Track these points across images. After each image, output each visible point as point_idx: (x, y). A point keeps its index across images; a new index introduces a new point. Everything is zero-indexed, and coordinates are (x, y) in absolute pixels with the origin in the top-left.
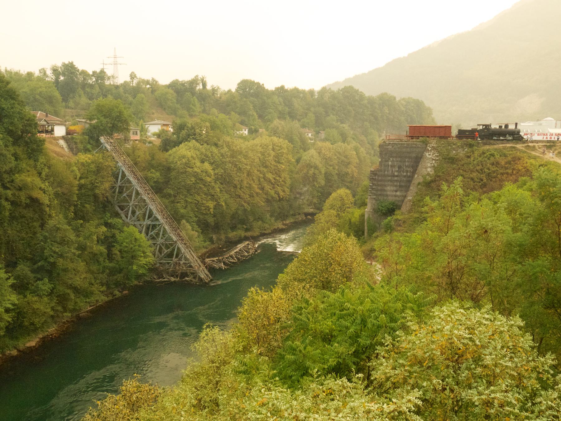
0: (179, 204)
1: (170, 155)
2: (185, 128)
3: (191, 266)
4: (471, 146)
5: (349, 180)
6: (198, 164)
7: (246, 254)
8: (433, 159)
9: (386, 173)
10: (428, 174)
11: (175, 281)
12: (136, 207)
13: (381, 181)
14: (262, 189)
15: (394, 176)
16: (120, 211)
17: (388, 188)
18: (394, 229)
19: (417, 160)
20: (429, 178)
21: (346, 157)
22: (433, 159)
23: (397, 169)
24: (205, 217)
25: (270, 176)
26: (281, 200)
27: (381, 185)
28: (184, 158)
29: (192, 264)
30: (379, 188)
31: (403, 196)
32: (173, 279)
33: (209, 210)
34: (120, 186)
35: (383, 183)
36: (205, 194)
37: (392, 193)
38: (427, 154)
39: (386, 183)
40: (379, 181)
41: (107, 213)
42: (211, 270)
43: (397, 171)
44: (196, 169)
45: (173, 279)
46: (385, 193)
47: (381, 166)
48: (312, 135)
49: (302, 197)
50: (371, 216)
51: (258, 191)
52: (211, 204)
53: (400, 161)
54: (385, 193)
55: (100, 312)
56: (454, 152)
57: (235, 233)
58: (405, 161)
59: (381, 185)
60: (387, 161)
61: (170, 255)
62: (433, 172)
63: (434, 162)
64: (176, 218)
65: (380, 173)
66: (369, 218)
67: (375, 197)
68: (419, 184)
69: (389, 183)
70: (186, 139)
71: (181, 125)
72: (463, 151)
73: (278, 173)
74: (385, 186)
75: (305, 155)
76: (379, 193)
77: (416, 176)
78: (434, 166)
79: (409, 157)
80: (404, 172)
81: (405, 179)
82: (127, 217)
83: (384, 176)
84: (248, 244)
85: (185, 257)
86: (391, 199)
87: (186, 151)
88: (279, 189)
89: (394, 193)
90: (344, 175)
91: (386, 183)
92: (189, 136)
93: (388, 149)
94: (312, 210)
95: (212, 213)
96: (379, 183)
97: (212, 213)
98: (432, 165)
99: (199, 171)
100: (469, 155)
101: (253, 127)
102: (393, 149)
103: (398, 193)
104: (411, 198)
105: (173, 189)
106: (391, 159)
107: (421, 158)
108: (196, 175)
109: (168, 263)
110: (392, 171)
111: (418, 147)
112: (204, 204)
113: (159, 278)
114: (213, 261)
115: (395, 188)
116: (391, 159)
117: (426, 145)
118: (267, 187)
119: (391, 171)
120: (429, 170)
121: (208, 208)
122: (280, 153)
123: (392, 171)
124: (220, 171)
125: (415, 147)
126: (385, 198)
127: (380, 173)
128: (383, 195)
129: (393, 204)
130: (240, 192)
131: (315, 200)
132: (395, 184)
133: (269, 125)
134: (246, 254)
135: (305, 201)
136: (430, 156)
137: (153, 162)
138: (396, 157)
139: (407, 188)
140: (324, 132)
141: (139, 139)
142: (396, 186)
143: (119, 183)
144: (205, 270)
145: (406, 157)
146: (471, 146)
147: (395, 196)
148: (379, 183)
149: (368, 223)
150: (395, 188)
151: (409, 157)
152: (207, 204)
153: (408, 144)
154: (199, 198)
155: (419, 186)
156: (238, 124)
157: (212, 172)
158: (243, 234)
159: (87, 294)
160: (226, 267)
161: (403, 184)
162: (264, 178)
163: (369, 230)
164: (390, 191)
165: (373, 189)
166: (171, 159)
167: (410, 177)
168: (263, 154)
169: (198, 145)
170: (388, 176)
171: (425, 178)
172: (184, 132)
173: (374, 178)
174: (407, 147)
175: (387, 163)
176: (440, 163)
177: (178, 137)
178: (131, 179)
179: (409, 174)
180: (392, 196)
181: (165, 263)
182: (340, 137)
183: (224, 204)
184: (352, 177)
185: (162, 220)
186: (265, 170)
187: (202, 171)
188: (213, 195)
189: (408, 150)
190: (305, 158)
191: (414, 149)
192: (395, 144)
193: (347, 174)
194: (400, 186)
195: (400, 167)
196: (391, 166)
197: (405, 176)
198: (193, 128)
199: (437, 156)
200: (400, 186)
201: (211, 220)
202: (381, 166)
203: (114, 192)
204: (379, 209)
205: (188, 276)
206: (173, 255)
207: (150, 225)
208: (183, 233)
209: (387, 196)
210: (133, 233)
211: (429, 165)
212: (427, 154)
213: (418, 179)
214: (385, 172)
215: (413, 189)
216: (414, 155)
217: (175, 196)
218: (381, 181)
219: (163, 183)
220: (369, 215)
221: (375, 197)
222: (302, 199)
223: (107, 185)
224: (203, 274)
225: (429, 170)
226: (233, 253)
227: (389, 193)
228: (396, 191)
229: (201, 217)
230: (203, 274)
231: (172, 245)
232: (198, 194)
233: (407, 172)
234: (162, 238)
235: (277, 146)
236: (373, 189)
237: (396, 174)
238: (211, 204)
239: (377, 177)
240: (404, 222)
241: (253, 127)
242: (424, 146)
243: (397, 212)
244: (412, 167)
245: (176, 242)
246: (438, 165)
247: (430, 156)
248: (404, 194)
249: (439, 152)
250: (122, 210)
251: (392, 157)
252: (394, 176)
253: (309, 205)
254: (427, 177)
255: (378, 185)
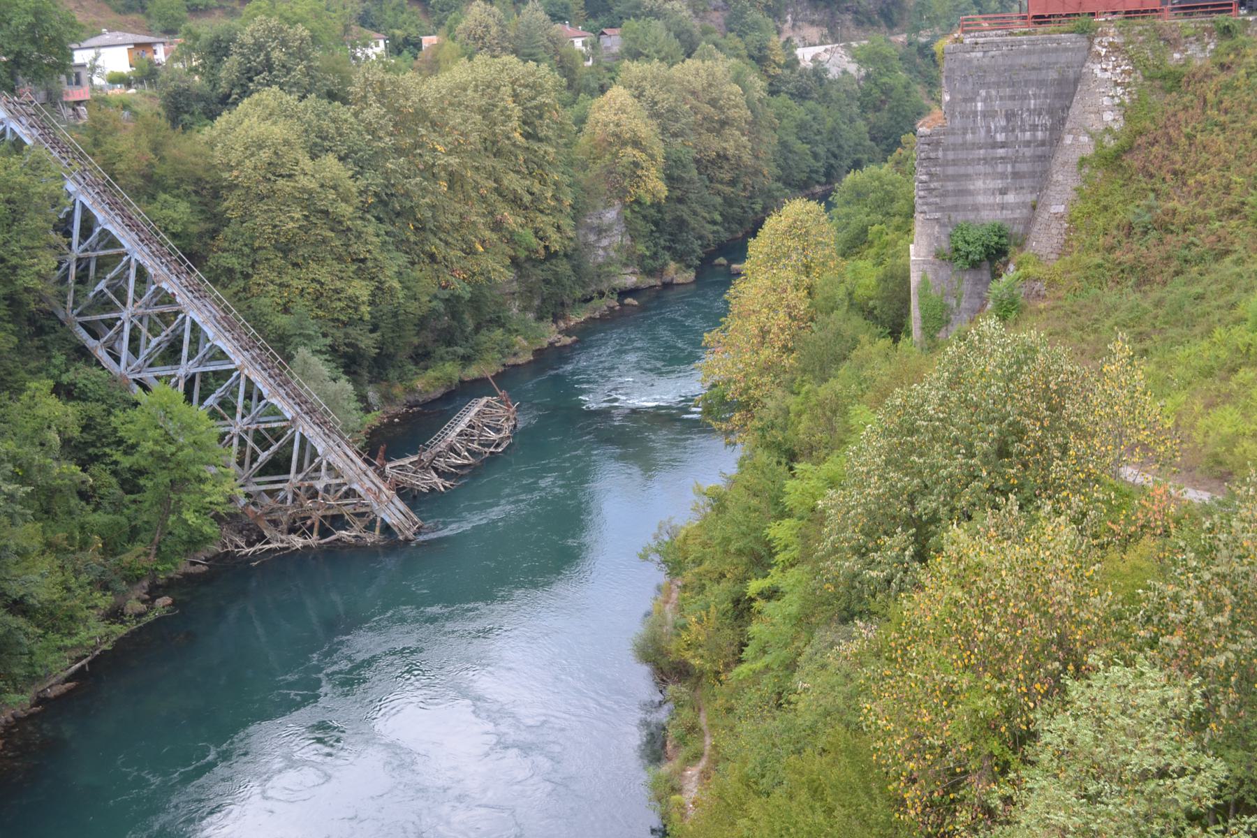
0: (263, 300)
1: (211, 144)
2: (233, 47)
3: (351, 493)
4: (1227, 32)
5: (727, 177)
6: (306, 163)
7: (493, 436)
8: (1117, 84)
9: (969, 137)
10: (1108, 130)
11: (306, 547)
12: (141, 320)
13: (955, 163)
14: (497, 226)
15: (995, 145)
16: (90, 343)
17: (979, 184)
18: (1025, 307)
19: (1067, 89)
20: (1111, 143)
21: (713, 102)
22: (1117, 84)
23: (1003, 123)
24: (347, 335)
25: (513, 182)
26: (551, 255)
27: (955, 178)
28: (260, 147)
29: (355, 486)
30: (950, 186)
31: (1024, 204)
32: (298, 542)
33: (356, 309)
34: (79, 260)
35: (962, 170)
36: (340, 259)
37: (991, 200)
38: (1097, 69)
39: (970, 170)
40: (946, 164)
41: (55, 352)
42: (407, 495)
43: (1004, 129)
44: (304, 181)
45: (298, 542)
46: (969, 200)
47: (953, 116)
48: (584, 44)
49: (605, 242)
50: (930, 276)
51: (487, 234)
52: (361, 289)
53: (1012, 98)
54: (969, 200)
55: (97, 674)
56: (1177, 56)
57: (431, 373)
58: (1025, 97)
59: (955, 178)
60: (973, 100)
61: (279, 466)
62: (1121, 122)
63: (1119, 90)
64: (279, 348)
65: (951, 139)
66: (924, 282)
67: (938, 215)
68: (1083, 162)
69: (981, 168)
70: (244, 86)
71: (217, 40)
72: (1203, 50)
73: (535, 167)
74: (967, 177)
75: (600, 108)
76: (950, 201)
77: (1068, 140)
78: (1121, 104)
79: (1041, 83)
80: (1023, 131)
81: (1028, 152)
82: (117, 360)
83: (964, 146)
84: (488, 405)
85: (330, 467)
86: (990, 217)
87: (256, 126)
88: (542, 221)
89: (998, 199)
90: (713, 162)
91: (970, 170)
92: (249, 74)
93: (970, 61)
94: (634, 279)
95: (367, 317)
96: (951, 170)
97: (367, 317)
98: (1117, 101)
99: (313, 185)
100: (1225, 60)
101: (398, 32)
102: (986, 61)
103: (1011, 198)
104: (1061, 209)
105: (239, 253)
106: (983, 93)
107: (1077, 81)
108: (306, 199)
109: (271, 494)
110: (989, 130)
111: (1066, 50)
112: (342, 290)
113: (250, 544)
114: (402, 468)
115: (999, 184)
116: (983, 93)
117: (1091, 40)
118: (512, 220)
119: (983, 132)
120: (1108, 116)
121: (353, 301)
122: (536, 107)
123: (989, 130)
124: (373, 180)
125: (1056, 50)
126: (971, 216)
127: (951, 139)
128: (965, 208)
129: (1000, 232)
130: (434, 245)
131: (641, 248)
132: (1000, 168)
133: (457, 21)
134: (493, 436)
135: (612, 254)
136: (1108, 74)
137: (160, 170)
138: (998, 85)
139: (1041, 179)
140: (617, 31)
141: (87, 97)
142: (1003, 176)
143: (77, 251)
144: (397, 500)
145: (1027, 83)
146: (1227, 32)
147: (1003, 207)
148: (951, 170)
149: (923, 295)
150: (999, 184)
151: (1041, 83)
152: (350, 291)
153: (1033, 43)
154: (322, 273)
155: (1086, 170)
156: (355, 29)
157: (353, 187)
158: (452, 371)
159: (55, 620)
160: (447, 484)
161: (1023, 167)
162: (498, 191)
163: (925, 319)
164: (985, 192)
165: (930, 190)
166: (218, 156)
167: (1043, 143)
168: (485, 112)
169: (291, 99)
170: (976, 146)
171: (1099, 144)
172: (232, 63)
173: (932, 155)
174: (1029, 52)
175: (969, 107)
176: (1138, 92)
177: (214, 84)
178: (116, 230)
179: (1040, 135)
180: (992, 207)
181: (259, 493)
182: (677, 43)
183: (396, 284)
184: (738, 167)
185: (238, 359)
186: (499, 164)
187: (322, 186)
188: (363, 261)
189: (1034, 60)
190: (601, 116)
191: (1053, 58)
192: (992, 43)
193: (723, 157)
194: (1016, 175)
195: (1010, 116)
196: (985, 115)
197: (1027, 144)
198: (259, 47)
199: (1129, 73)
200: (1016, 175)
201: (368, 342)
202: (953, 116)
203: (64, 279)
204: (957, 250)
205: (345, 525)
206: (289, 459)
207: (194, 376)
208: (308, 389)
209: (976, 208)
210: (158, 406)
211: (1106, 101)
212: (1097, 69)
213: (1078, 144)
214: (964, 134)
215: (1064, 180)
216: (1053, 75)
217: (247, 276)
218: (955, 163)
219: (200, 236)
220: (925, 272)
221: (938, 215)
222: (604, 248)
223: (47, 261)
224: (394, 513)
225: (1108, 116)
226: (452, 436)
227: (981, 199)
228: (1003, 192)
229: (339, 334)
230: (394, 513)
231: (277, 434)
232: (318, 260)
233: (1034, 128)
234: (243, 417)
235: (526, 86)
236: (930, 190)
237: (1000, 137)
238: (361, 289)
239: (940, 154)
240: (1052, 284)
241: (398, 32)
242: (1085, 43)
243: (1015, 255)
244: (1051, 112)
245: (294, 420)
246: (1132, 100)
247: (1108, 74)
248: (1030, 198)
249: (1131, 58)
250: (96, 337)
251: (982, 85)
252: (995, 145)
253: (626, 265)
254: (1107, 138)
255: (947, 178)
